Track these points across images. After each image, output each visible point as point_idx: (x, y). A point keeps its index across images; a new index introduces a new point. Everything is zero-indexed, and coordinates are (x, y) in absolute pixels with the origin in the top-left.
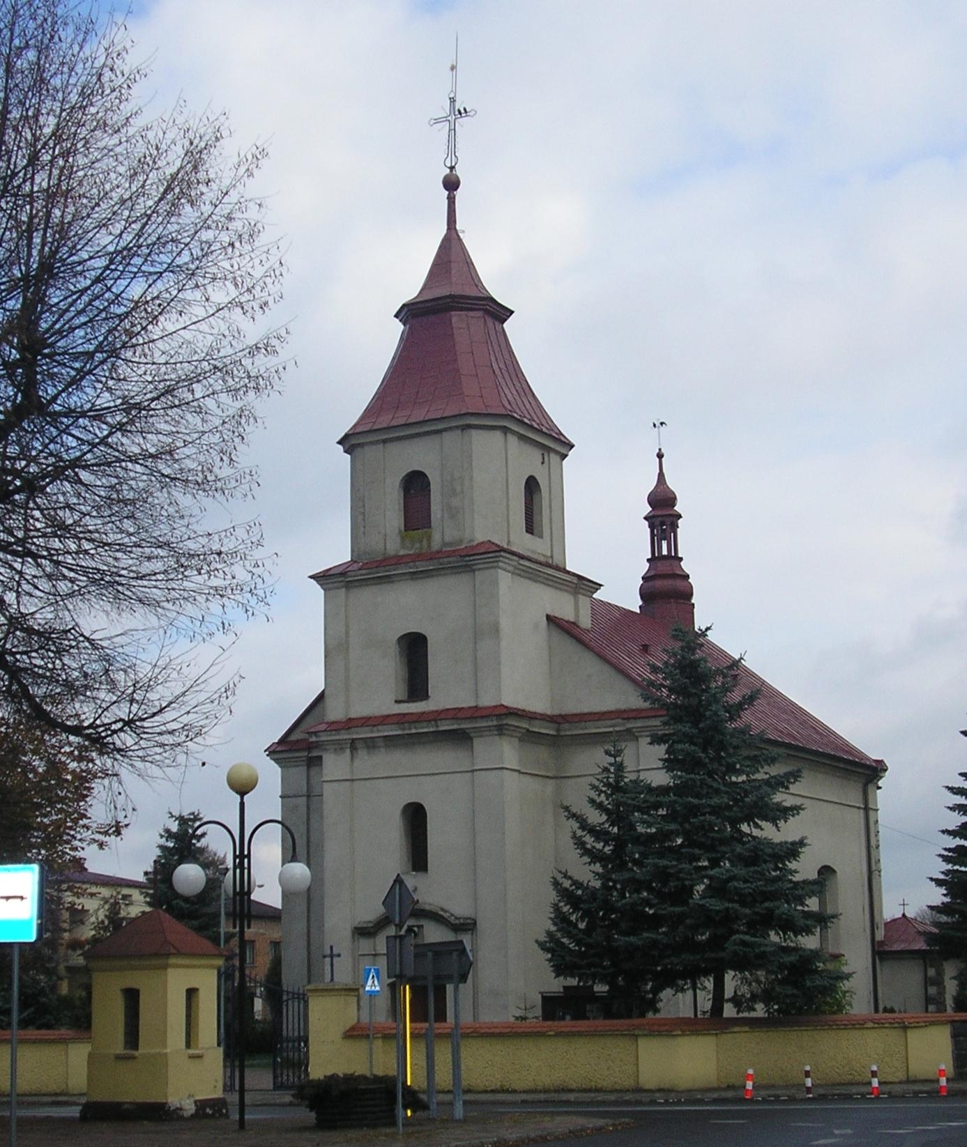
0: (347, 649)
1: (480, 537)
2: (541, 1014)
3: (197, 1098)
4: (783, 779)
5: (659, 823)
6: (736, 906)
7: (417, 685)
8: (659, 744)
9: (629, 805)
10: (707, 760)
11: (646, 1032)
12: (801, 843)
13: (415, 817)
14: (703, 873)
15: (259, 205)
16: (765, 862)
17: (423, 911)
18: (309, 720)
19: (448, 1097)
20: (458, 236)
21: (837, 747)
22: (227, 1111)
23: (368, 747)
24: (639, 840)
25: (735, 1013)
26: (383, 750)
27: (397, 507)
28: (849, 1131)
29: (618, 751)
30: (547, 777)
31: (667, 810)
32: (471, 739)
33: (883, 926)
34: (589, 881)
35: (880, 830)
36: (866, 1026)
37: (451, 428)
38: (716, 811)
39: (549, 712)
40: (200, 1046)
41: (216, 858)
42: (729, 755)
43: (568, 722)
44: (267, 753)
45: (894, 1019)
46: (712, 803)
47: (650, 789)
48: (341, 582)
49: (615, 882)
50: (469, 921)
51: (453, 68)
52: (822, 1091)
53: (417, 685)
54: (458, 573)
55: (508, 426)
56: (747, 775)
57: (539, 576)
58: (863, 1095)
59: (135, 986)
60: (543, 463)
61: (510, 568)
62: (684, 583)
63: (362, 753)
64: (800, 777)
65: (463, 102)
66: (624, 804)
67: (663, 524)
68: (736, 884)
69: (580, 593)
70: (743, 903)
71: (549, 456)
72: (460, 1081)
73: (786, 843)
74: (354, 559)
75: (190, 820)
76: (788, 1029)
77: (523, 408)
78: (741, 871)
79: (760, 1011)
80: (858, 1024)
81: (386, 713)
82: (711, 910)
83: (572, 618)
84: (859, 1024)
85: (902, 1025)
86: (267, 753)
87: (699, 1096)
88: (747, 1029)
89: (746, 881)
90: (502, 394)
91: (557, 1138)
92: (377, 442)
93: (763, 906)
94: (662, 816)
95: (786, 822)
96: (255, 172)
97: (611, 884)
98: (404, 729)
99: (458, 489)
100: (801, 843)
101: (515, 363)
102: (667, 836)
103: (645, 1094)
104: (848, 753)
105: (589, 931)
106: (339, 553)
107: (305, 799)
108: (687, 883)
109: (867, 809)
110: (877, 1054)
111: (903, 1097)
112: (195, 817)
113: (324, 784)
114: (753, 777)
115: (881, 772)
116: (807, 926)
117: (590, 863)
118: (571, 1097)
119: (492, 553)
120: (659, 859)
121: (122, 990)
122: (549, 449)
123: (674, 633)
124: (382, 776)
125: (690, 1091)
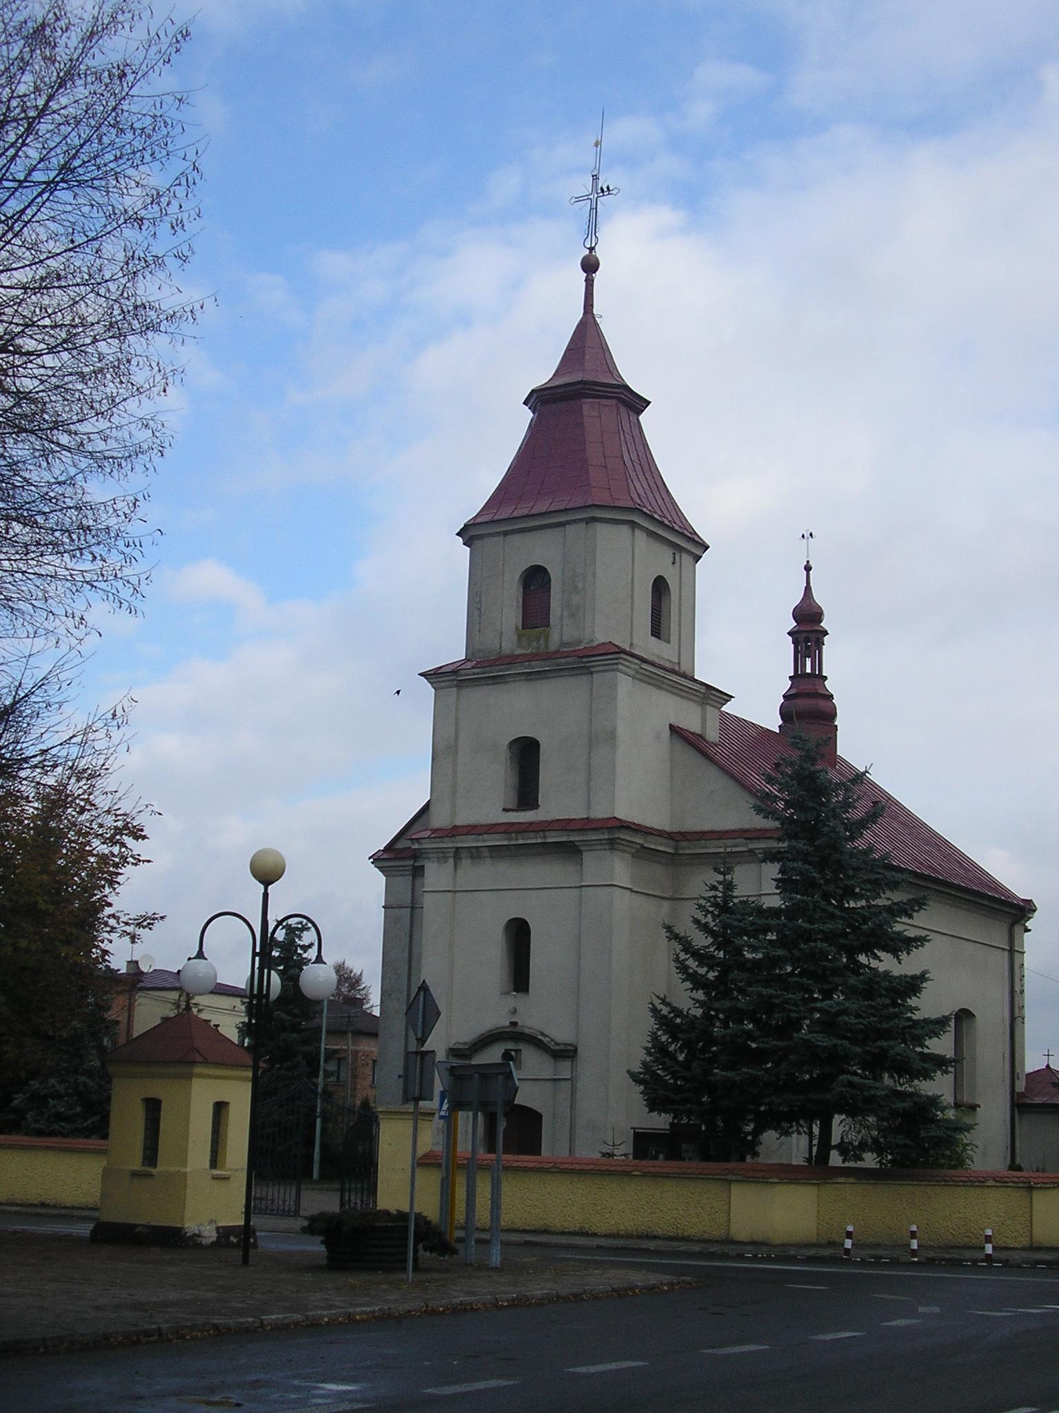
0: (456, 751)
1: (601, 638)
2: (631, 1151)
3: (220, 1225)
4: (907, 907)
5: (766, 948)
6: (845, 1042)
7: (527, 794)
8: (772, 861)
9: (735, 927)
10: (822, 881)
11: (741, 1178)
12: (923, 977)
13: (519, 933)
14: (812, 1005)
15: (180, 100)
16: (881, 996)
17: (522, 1034)
18: (417, 827)
19: (486, 1236)
20: (595, 320)
21: (982, 884)
22: (255, 1241)
23: (472, 857)
24: (743, 965)
25: (841, 1161)
26: (488, 861)
27: (515, 604)
28: (936, 1310)
29: (728, 868)
30: (663, 898)
31: (777, 935)
32: (581, 852)
33: (1024, 1077)
34: (690, 1009)
35: (1025, 974)
36: (986, 1184)
37: (575, 521)
38: (830, 937)
39: (668, 829)
40: (227, 1166)
41: (352, 975)
42: (848, 877)
43: (687, 840)
44: (372, 860)
45: (1018, 1178)
46: (825, 929)
47: (760, 911)
48: (454, 680)
49: (717, 1011)
50: (570, 1048)
51: (596, 145)
52: (931, 1254)
53: (527, 794)
54: (577, 674)
55: (637, 521)
56: (867, 901)
57: (664, 683)
58: (975, 1262)
59: (160, 1097)
60: (673, 563)
61: (630, 672)
62: (828, 703)
63: (466, 863)
64: (924, 904)
65: (606, 180)
66: (730, 926)
67: (807, 640)
68: (846, 1018)
69: (708, 704)
70: (853, 1041)
71: (681, 556)
72: (498, 1218)
73: (906, 976)
74: (469, 658)
75: (298, 929)
76: (899, 1182)
77: (654, 503)
78: (853, 1005)
79: (870, 1160)
80: (979, 1182)
81: (494, 822)
82: (818, 1046)
83: (698, 730)
84: (978, 1181)
85: (1027, 1185)
86: (372, 860)
87: (793, 1253)
88: (852, 1180)
89: (857, 1016)
90: (632, 487)
91: (596, 1298)
92: (497, 534)
93: (876, 1044)
94: (770, 941)
95: (908, 953)
96: (174, 57)
97: (713, 1013)
98: (511, 839)
99: (580, 586)
100: (923, 977)
101: (649, 456)
102: (773, 962)
103: (733, 1247)
104: (996, 890)
105: (686, 1065)
106: (454, 650)
107: (409, 909)
108: (792, 1015)
109: (1012, 951)
110: (999, 1216)
111: (1019, 1267)
112: (303, 926)
113: (425, 894)
114: (873, 903)
115: (1029, 913)
116: (925, 1069)
117: (692, 990)
118: (652, 1245)
119: (612, 654)
120: (763, 987)
121: (143, 1099)
122: (680, 549)
123: (793, 740)
124: (487, 888)
125: (783, 1245)
